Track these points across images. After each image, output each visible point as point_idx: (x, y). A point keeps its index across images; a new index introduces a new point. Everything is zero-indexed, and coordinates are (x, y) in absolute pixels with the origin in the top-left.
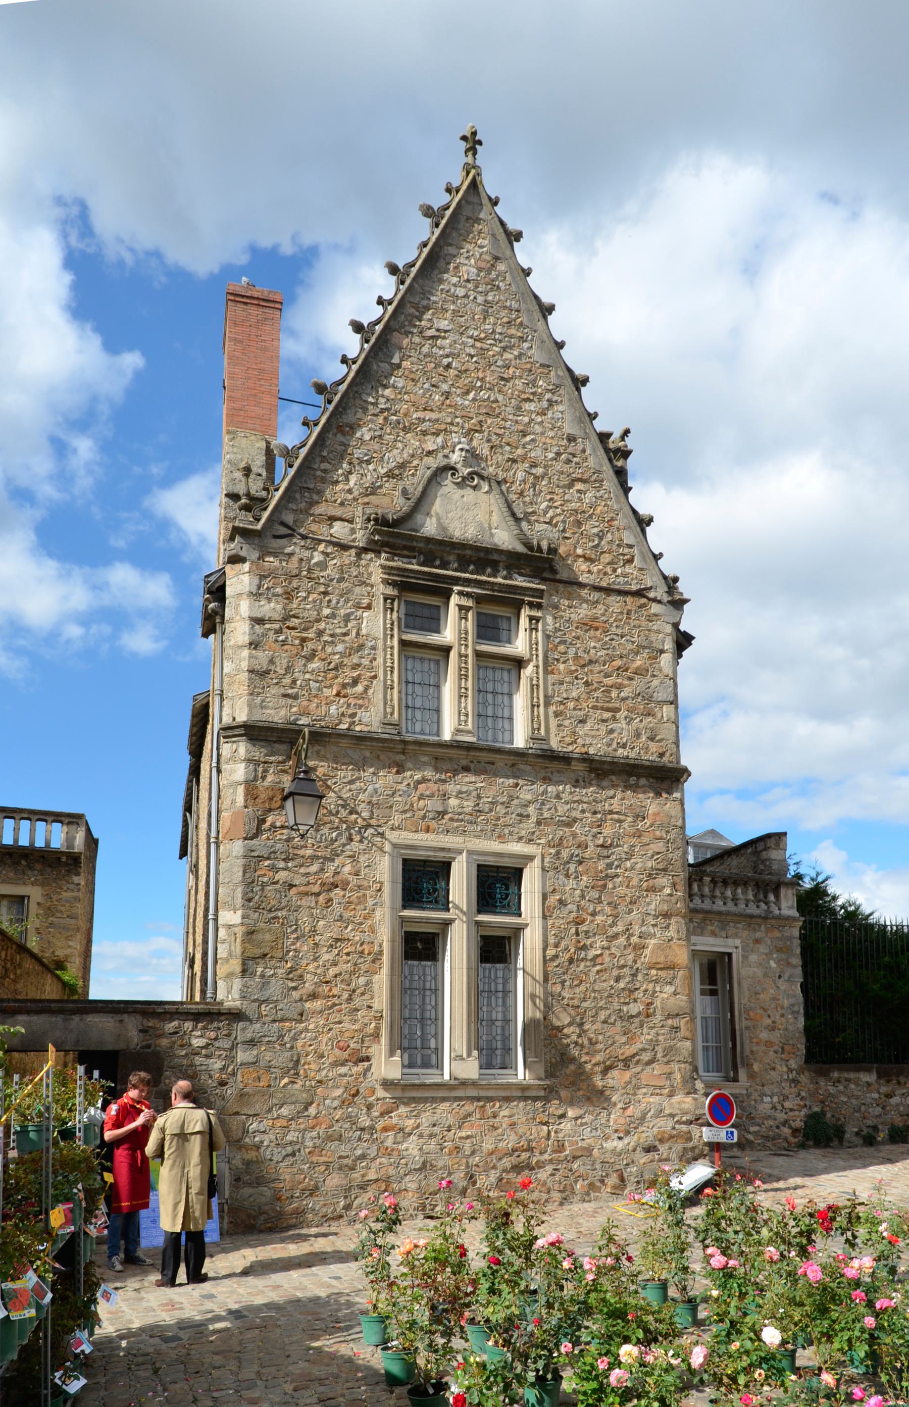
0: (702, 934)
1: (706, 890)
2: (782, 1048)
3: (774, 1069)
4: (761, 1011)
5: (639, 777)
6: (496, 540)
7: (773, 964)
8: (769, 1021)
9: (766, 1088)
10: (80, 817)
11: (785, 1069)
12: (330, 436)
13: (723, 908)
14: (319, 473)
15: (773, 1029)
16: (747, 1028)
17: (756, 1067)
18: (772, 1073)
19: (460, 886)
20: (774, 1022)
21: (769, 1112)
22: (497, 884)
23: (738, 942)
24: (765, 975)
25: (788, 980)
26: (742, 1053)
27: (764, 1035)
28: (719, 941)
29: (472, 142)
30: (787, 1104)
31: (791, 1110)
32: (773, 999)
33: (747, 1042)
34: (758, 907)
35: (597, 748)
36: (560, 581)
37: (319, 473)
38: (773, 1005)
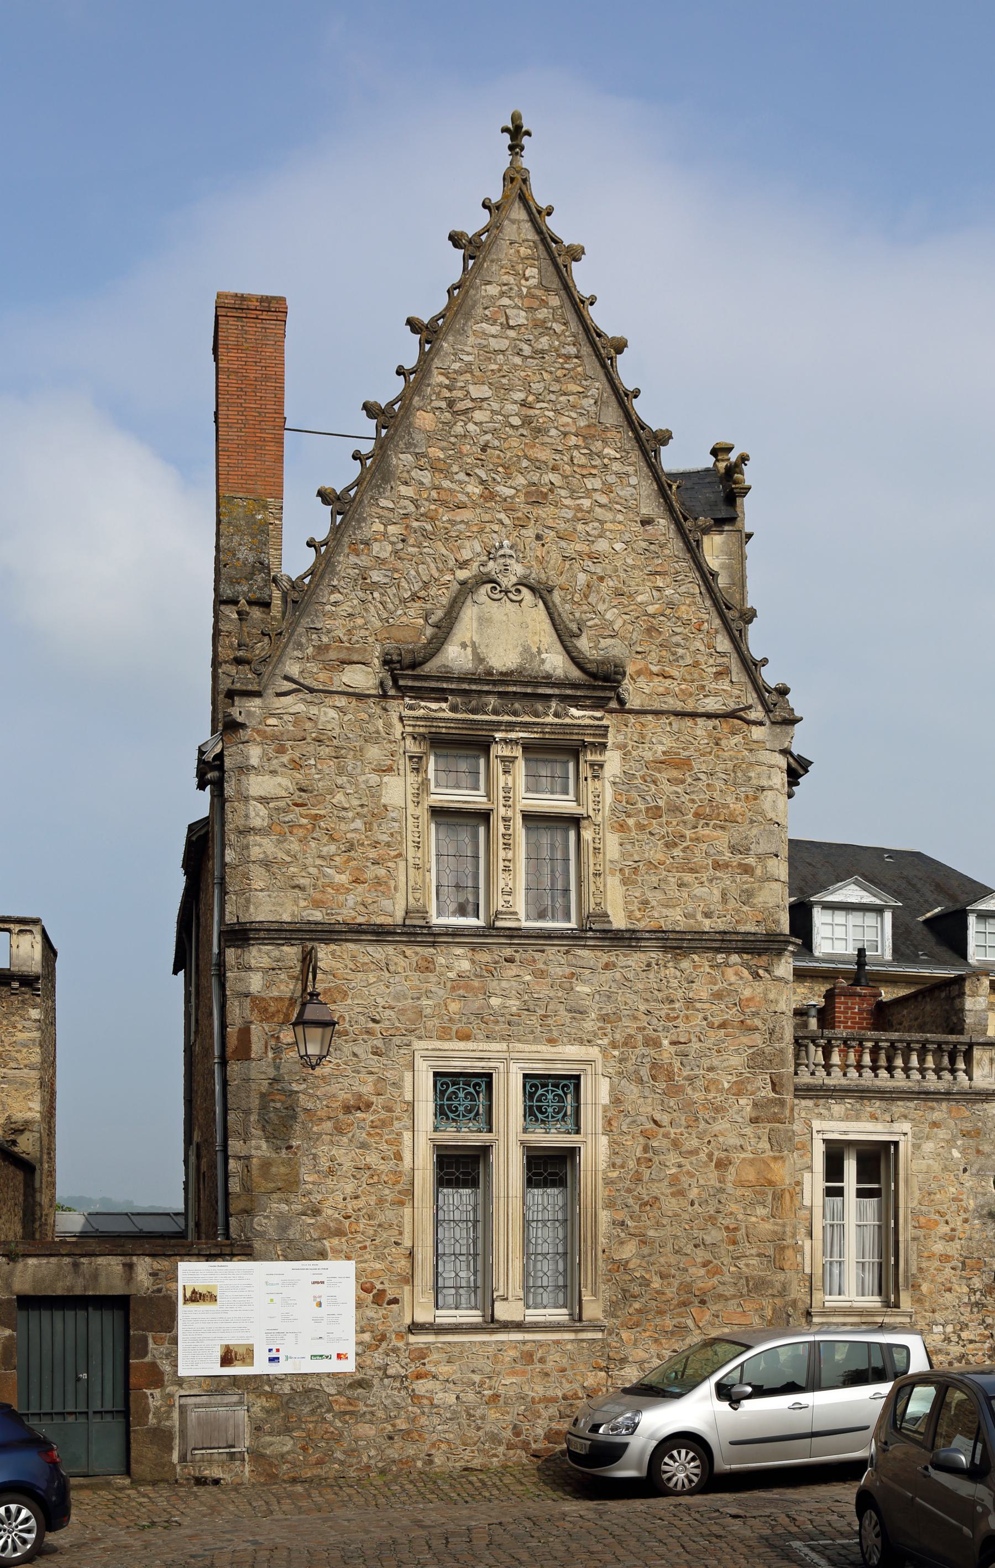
0: (858, 1118)
1: (867, 1059)
2: (963, 1263)
3: (950, 1290)
4: (937, 1217)
5: (728, 951)
6: (547, 667)
7: (956, 1154)
8: (946, 1229)
9: (937, 1315)
10: (36, 922)
11: (965, 1289)
12: (341, 559)
13: (890, 1084)
14: (328, 607)
15: (952, 1239)
16: (914, 1239)
17: (925, 1288)
18: (947, 1295)
19: (510, 1098)
20: (953, 1230)
21: (940, 1345)
22: (552, 1093)
23: (906, 1127)
24: (945, 1169)
25: (977, 1174)
26: (906, 1271)
27: (939, 1247)
28: (879, 1127)
29: (516, 132)
30: (964, 1335)
31: (971, 1342)
32: (954, 1200)
33: (913, 1256)
34: (939, 1078)
35: (675, 919)
36: (630, 712)
37: (328, 607)
38: (954, 1208)
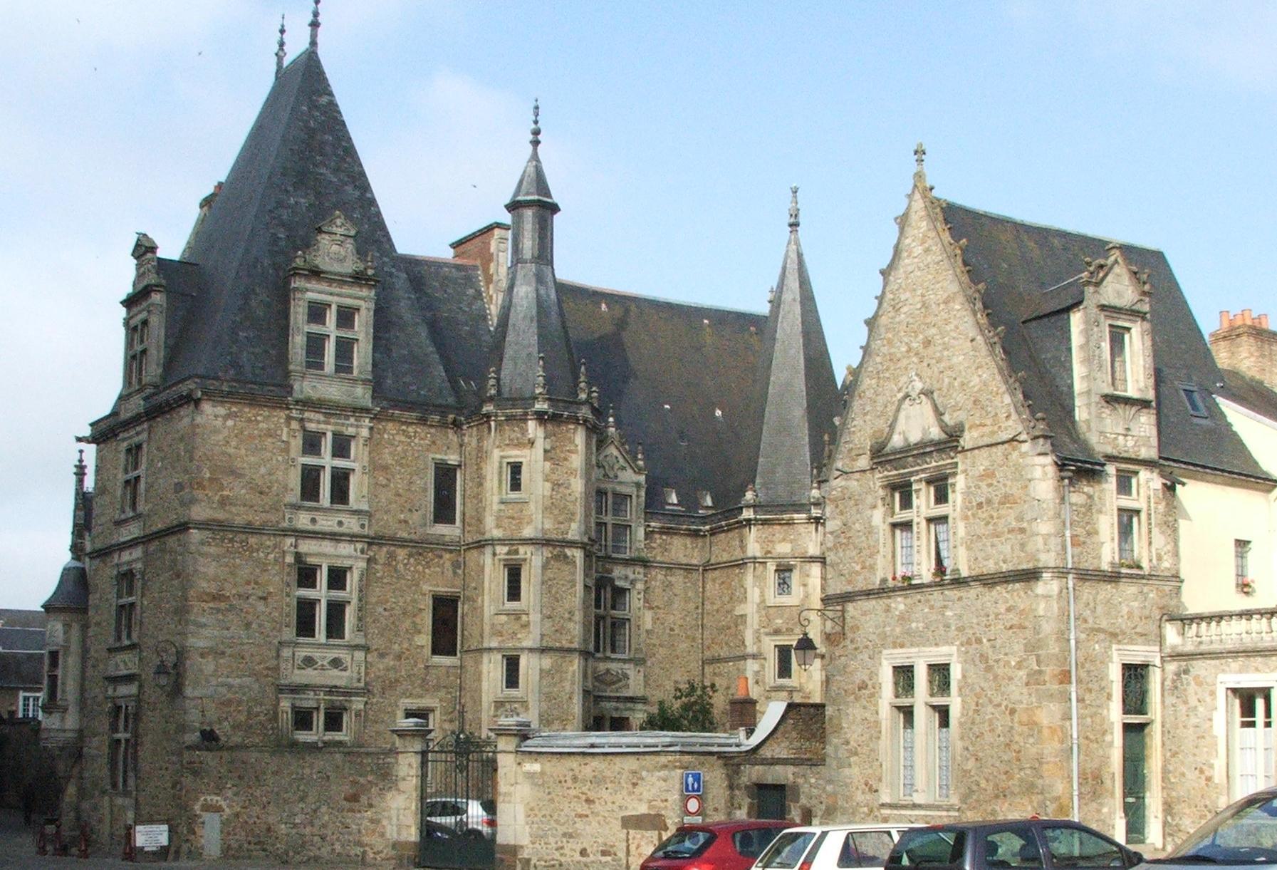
6: (932, 436)
